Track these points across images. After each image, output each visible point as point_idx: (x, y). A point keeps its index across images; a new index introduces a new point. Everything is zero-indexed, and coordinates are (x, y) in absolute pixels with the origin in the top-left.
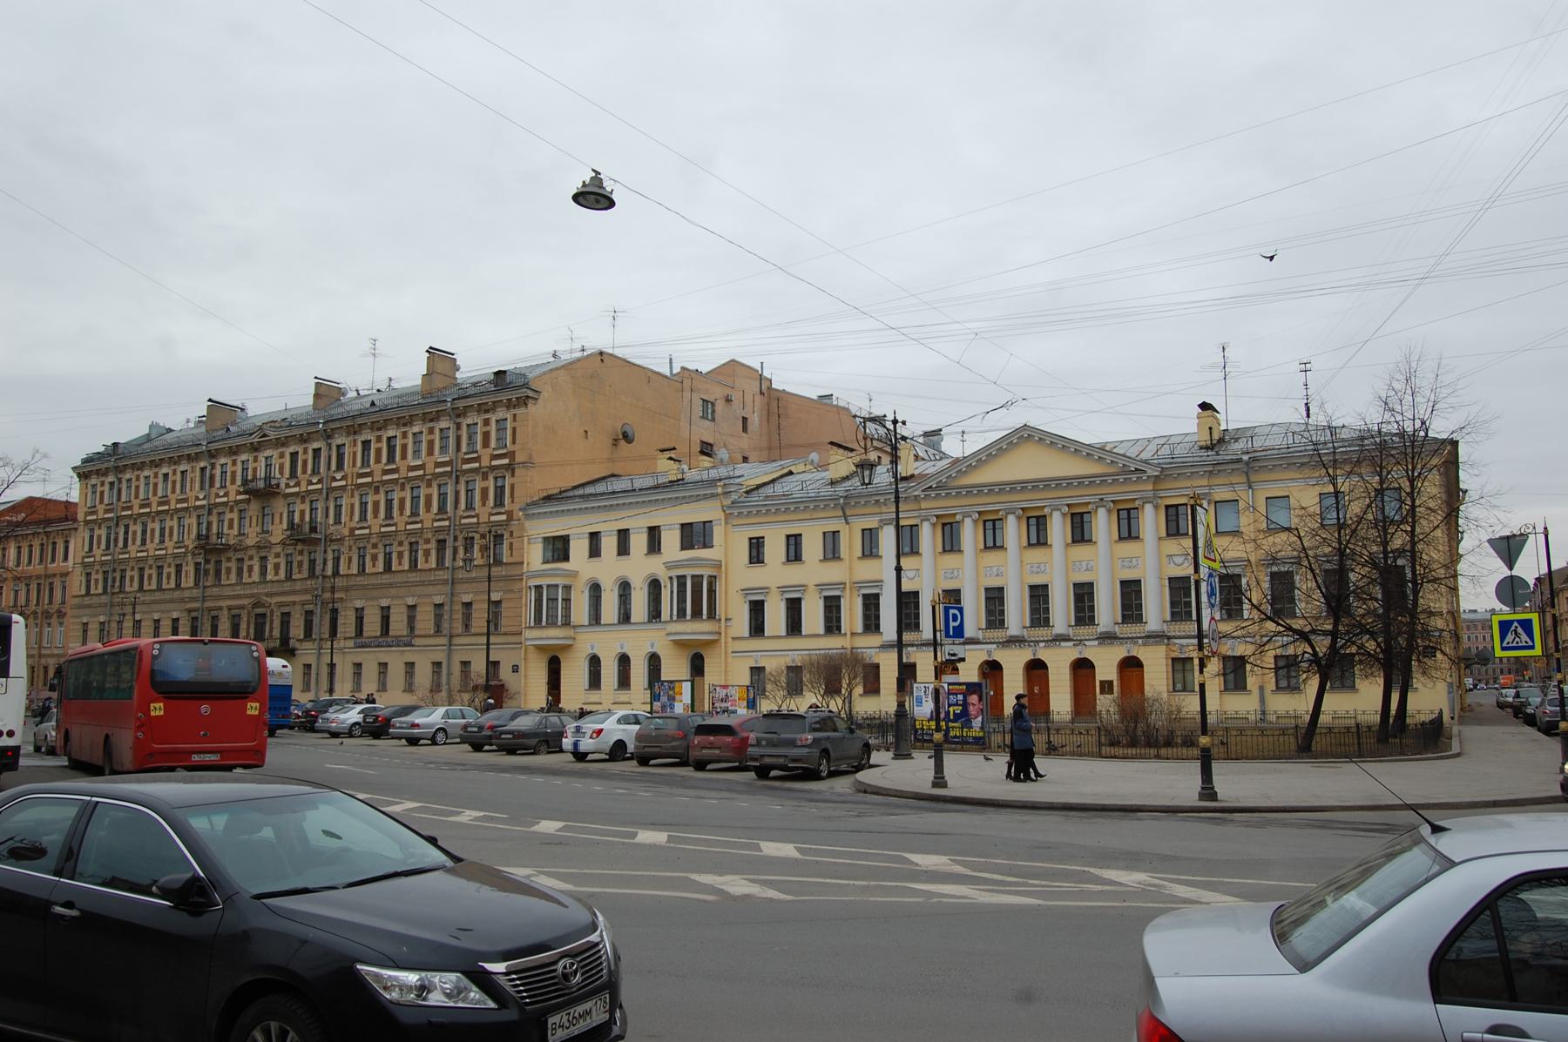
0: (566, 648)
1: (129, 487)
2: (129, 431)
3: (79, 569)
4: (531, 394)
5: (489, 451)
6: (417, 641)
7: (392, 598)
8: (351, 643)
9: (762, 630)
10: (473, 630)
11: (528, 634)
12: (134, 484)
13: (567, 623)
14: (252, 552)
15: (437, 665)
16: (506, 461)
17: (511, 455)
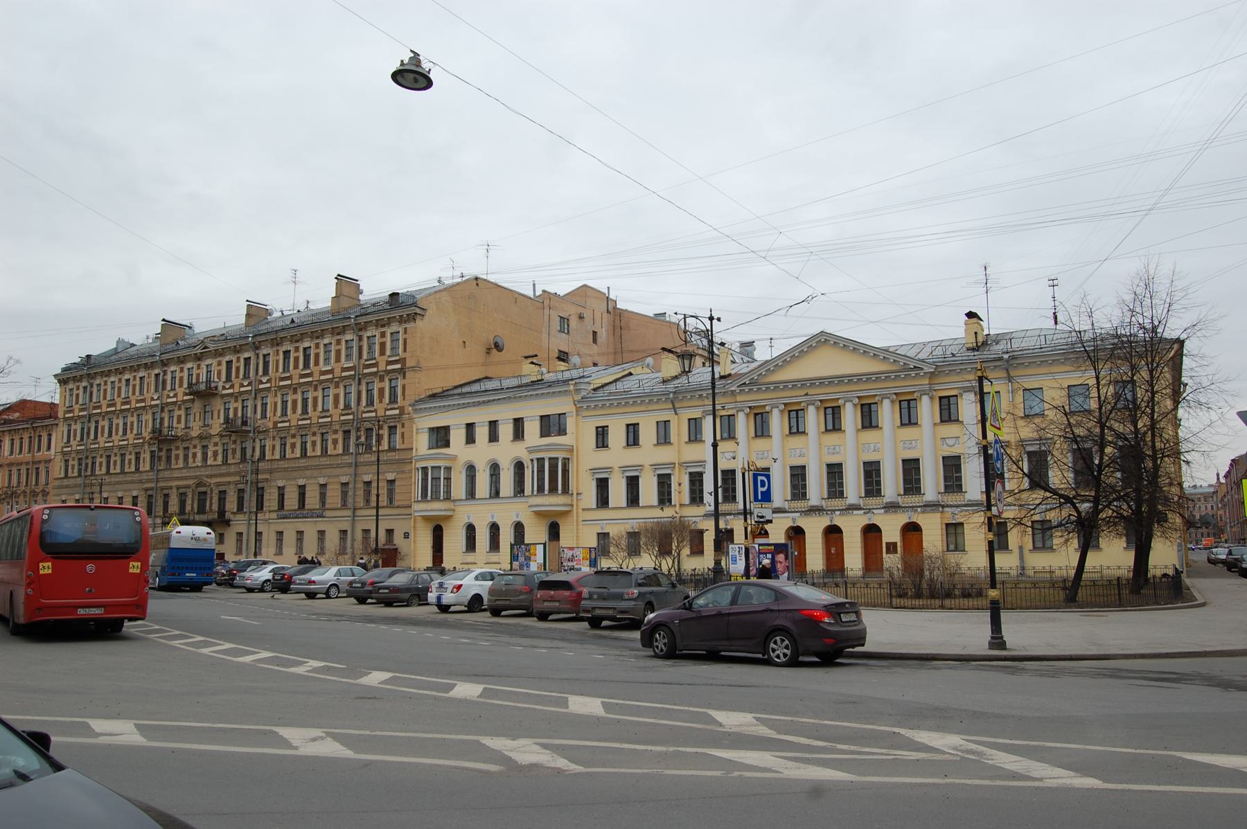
0: (448, 518)
2: (100, 346)
3: (59, 457)
4: (418, 311)
6: (327, 513)
8: (274, 515)
9: (607, 503)
11: (416, 507)
13: (448, 497)
14: (196, 442)
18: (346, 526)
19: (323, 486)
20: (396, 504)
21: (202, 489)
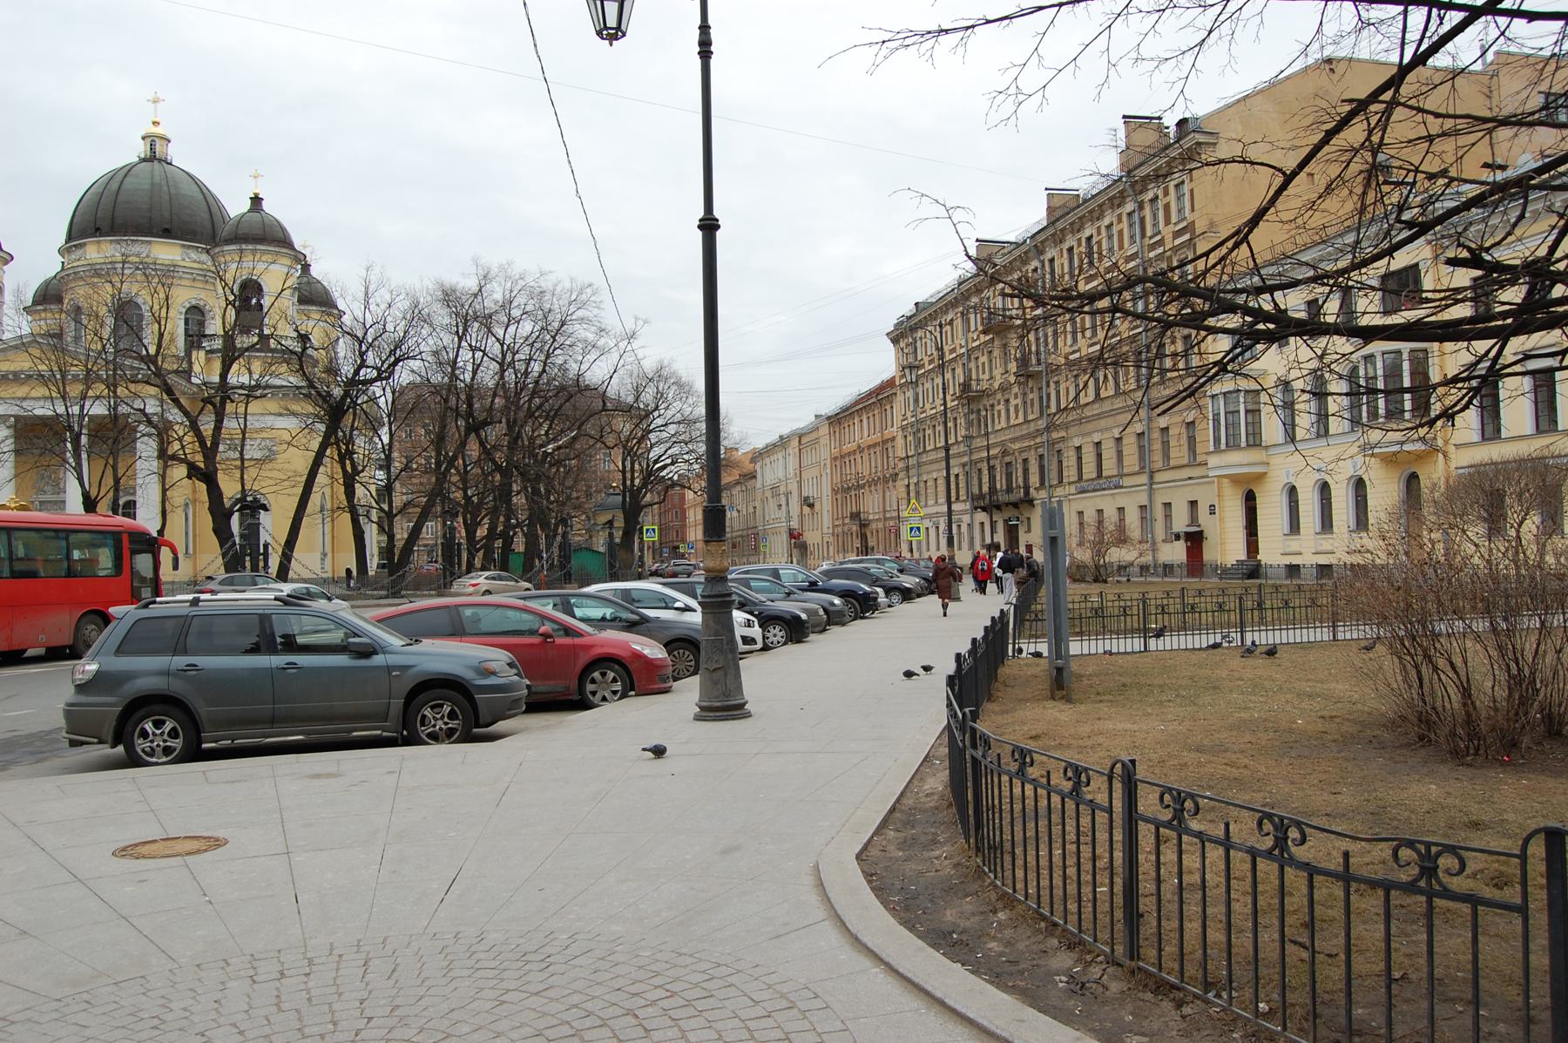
0: (1261, 477)
1: (1110, 237)
2: (908, 309)
4: (1201, 138)
5: (1171, 228)
6: (1126, 481)
7: (1101, 431)
8: (1073, 489)
9: (1498, 430)
10: (1172, 463)
11: (1213, 461)
12: (1115, 230)
13: (1255, 441)
15: (1143, 508)
16: (1187, 237)
17: (1190, 228)
18: (1144, 500)
19: (1098, 444)
20: (1172, 463)
21: (1007, 459)
